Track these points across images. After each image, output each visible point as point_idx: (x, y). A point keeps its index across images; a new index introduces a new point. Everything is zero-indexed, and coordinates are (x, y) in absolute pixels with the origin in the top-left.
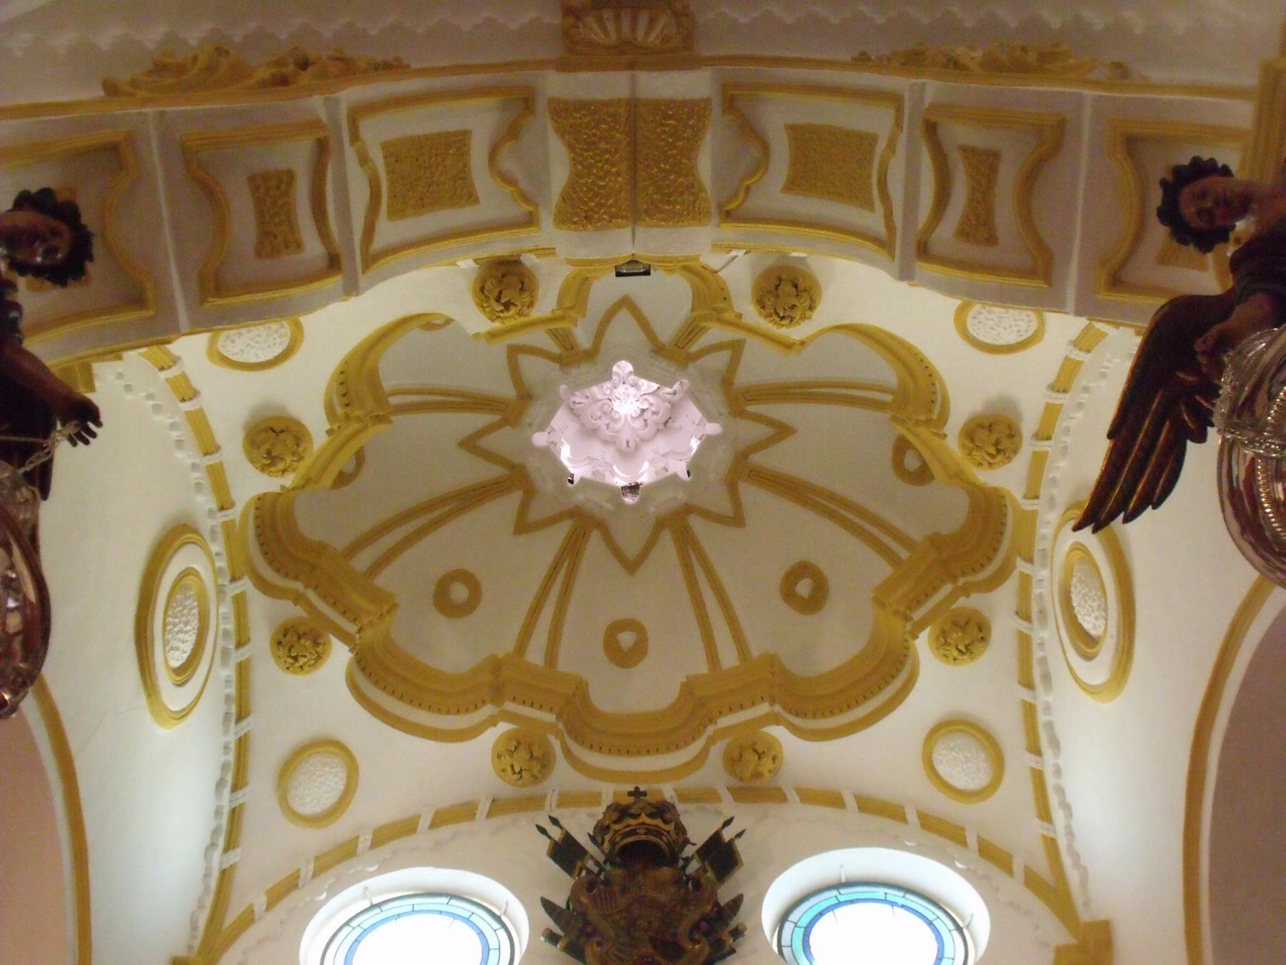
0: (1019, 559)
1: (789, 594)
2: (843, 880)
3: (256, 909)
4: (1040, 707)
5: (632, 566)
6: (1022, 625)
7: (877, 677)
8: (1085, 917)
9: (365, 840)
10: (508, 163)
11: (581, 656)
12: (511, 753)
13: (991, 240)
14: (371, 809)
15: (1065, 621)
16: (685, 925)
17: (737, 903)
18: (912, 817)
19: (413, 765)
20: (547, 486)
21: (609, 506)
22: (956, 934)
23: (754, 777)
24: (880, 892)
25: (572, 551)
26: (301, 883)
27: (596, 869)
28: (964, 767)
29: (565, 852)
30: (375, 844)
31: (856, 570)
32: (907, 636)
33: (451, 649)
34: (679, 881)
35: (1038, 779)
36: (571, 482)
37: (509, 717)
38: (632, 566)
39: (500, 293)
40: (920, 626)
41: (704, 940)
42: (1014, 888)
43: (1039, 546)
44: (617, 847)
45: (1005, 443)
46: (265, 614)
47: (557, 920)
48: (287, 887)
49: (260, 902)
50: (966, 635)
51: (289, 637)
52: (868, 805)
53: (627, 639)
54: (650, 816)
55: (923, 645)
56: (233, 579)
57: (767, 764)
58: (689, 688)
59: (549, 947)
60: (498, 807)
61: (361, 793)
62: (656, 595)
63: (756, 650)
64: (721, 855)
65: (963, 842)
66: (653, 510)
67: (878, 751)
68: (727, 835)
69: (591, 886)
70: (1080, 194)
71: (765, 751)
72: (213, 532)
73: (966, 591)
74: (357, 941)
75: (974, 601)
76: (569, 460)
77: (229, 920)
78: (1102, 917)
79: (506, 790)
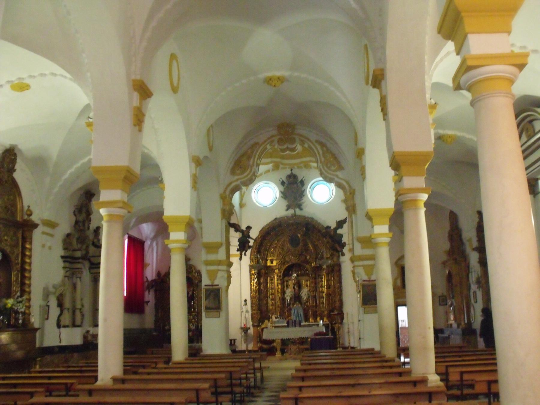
17: (304, 190)
29: (283, 183)
60: (273, 170)
64: (302, 183)
68: (303, 179)
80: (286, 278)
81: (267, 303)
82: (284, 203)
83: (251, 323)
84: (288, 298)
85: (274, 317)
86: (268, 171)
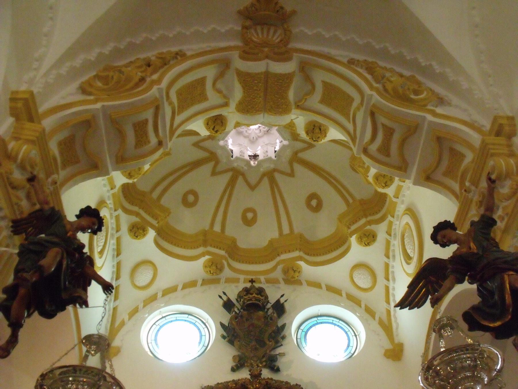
0: (389, 216)
1: (308, 205)
3: (125, 321)
4: (392, 244)
5: (252, 188)
6: (388, 237)
7: (335, 246)
8: (396, 341)
9: (160, 295)
10: (219, 85)
11: (235, 230)
12: (210, 267)
13: (388, 155)
14: (163, 282)
15: (402, 248)
16: (267, 335)
17: (284, 326)
18: (344, 295)
19: (175, 269)
20: (224, 160)
21: (246, 168)
22: (354, 337)
23: (291, 276)
24: (331, 319)
25: (232, 184)
27: (238, 312)
28: (362, 280)
29: (228, 305)
30: (163, 296)
31: (334, 204)
32: (348, 235)
33: (188, 222)
34: (266, 318)
35: (387, 289)
36: (232, 157)
37: (209, 253)
38: (252, 188)
39: (214, 127)
40: (351, 234)
41: (273, 341)
43: (397, 213)
44: (246, 304)
45: (388, 183)
46: (126, 220)
47: (225, 330)
48: (135, 312)
49: (126, 318)
50: (368, 238)
51: (134, 229)
53: (250, 215)
54: (257, 294)
55: (353, 239)
56: (115, 210)
57: (297, 274)
58: (271, 242)
60: (205, 282)
61: (158, 278)
62: (260, 199)
63: (296, 230)
64: (280, 308)
66: (262, 170)
67: (336, 272)
68: (282, 300)
70: (422, 142)
71: (297, 270)
72: (109, 197)
73: (369, 223)
74: (158, 331)
75: (373, 227)
76: (232, 144)
77: (117, 324)
78: (401, 342)
79: (208, 276)
82: (228, 354)
86: (191, 284)
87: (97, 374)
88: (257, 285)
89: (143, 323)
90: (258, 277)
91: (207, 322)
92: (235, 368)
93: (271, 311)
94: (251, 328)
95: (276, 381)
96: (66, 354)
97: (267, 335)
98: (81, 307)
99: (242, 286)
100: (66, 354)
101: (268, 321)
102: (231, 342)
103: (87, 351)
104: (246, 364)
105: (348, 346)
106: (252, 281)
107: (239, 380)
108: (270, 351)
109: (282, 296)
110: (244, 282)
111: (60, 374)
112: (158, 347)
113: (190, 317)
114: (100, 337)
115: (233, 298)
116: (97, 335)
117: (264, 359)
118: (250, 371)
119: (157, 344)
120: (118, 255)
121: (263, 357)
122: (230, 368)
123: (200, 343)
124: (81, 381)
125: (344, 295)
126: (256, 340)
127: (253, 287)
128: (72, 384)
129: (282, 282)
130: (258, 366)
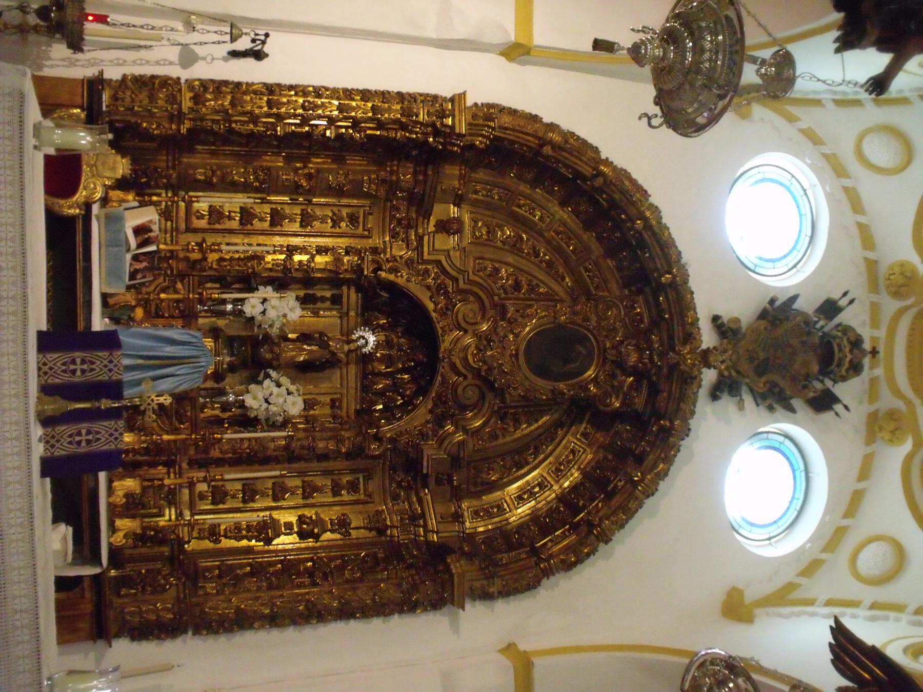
2: (810, 475)
4: (899, 615)
8: (757, 611)
9: (847, 183)
12: (902, 274)
14: (870, 187)
16: (777, 378)
17: (792, 410)
22: (767, 536)
23: (883, 425)
24: (800, 495)
26: (817, 146)
27: (818, 326)
28: (873, 559)
29: (830, 308)
30: (846, 189)
34: (807, 377)
41: (765, 389)
42: (789, 575)
44: (832, 340)
47: (784, 303)
49: (803, 125)
52: (857, 498)
54: (851, 361)
57: (887, 436)
59: (768, 299)
60: (872, 266)
64: (824, 402)
65: (825, 550)
68: (838, 407)
69: (807, 323)
71: (896, 436)
74: (781, 184)
77: (790, 108)
78: (756, 620)
79: (883, 270)
80: (352, 297)
81: (234, 187)
82: (741, 309)
83: (113, 74)
84: (252, 305)
85: (149, 216)
87: (729, 83)
88: (867, 361)
89: (795, 155)
90: (882, 364)
91: (798, 271)
92: (720, 322)
93: (818, 386)
94: (789, 350)
95: (696, 394)
96: (760, 24)
97: (777, 378)
98: (836, 41)
99: (866, 333)
100: (760, 24)
101: (801, 382)
102: (763, 315)
103: (763, 62)
104: (725, 341)
105: (752, 524)
106: (874, 352)
107: (699, 328)
108: (747, 384)
109: (846, 407)
110: (873, 339)
111: (727, 18)
112: (752, 185)
113: (808, 239)
114: (791, 81)
115: (844, 318)
116: (794, 74)
117: (734, 373)
118: (715, 348)
119: (757, 182)
120: (839, 103)
121: (738, 372)
122: (719, 313)
123: (761, 259)
124: (717, 57)
125: (845, 522)
126: (768, 359)
127: (863, 353)
128: (711, 42)
129: (872, 408)
130: (722, 362)
